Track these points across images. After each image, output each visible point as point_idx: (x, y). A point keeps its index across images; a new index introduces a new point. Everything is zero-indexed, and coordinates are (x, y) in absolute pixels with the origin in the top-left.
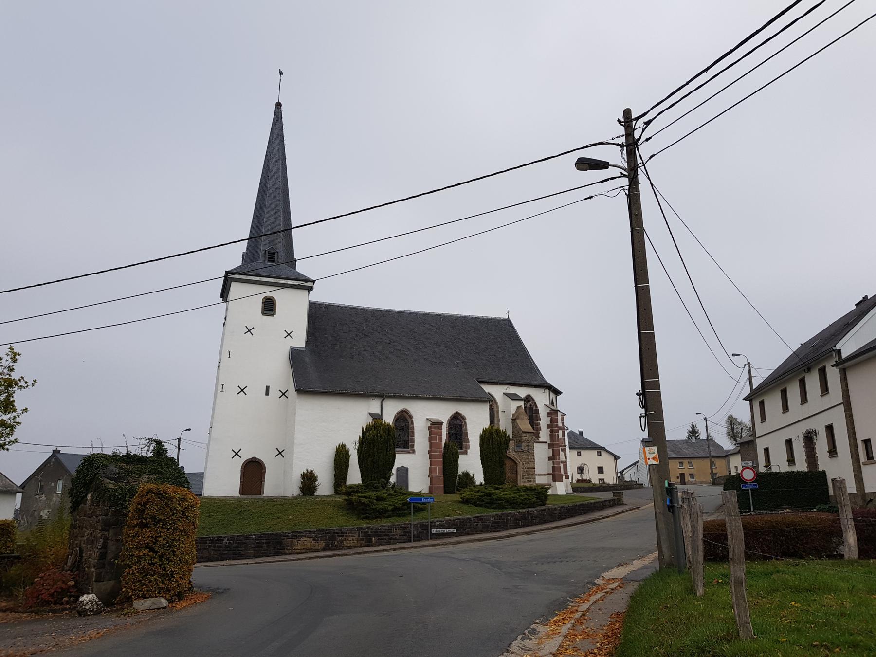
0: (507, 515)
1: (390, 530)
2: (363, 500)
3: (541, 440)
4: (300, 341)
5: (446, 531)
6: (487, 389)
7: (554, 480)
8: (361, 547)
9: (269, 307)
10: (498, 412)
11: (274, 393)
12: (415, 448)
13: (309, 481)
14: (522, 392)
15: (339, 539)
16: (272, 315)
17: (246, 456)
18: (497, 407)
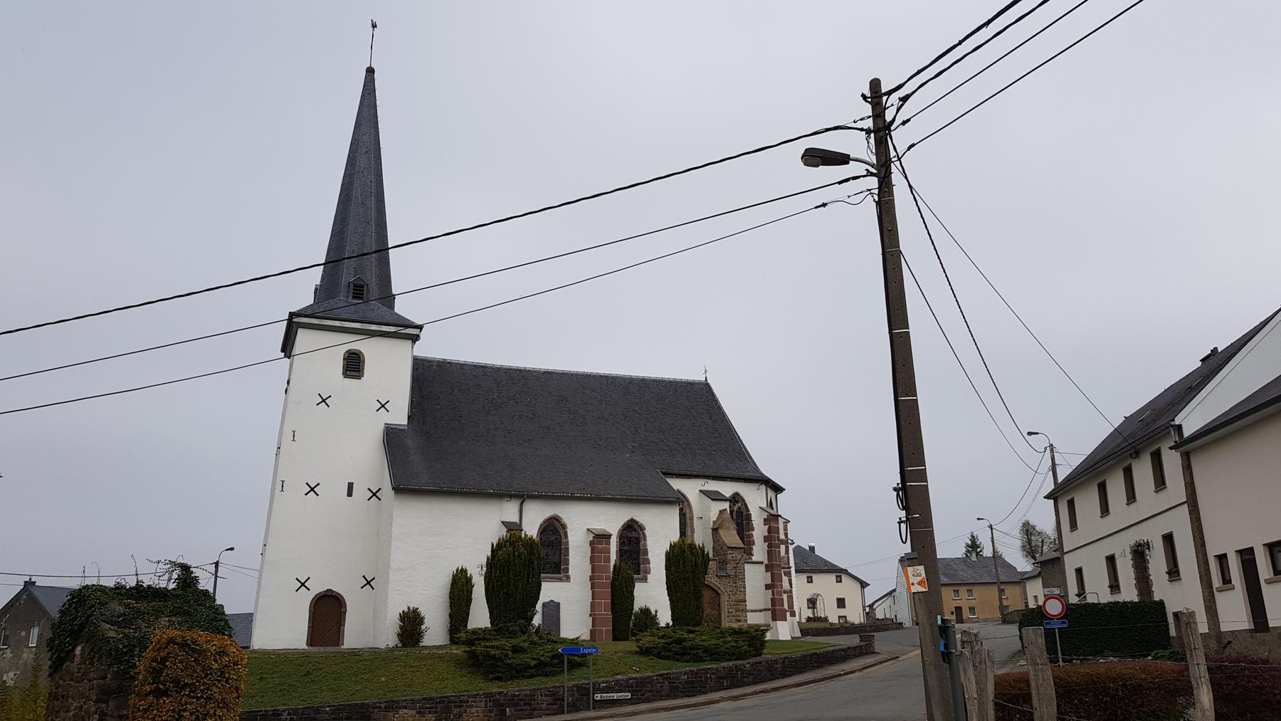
2: (493, 652)
3: (754, 559)
4: (399, 415)
5: (615, 696)
7: (774, 619)
9: (354, 365)
10: (692, 519)
11: (360, 492)
12: (570, 572)
13: (411, 623)
14: (727, 489)
15: (456, 711)
16: (359, 377)
17: (317, 588)
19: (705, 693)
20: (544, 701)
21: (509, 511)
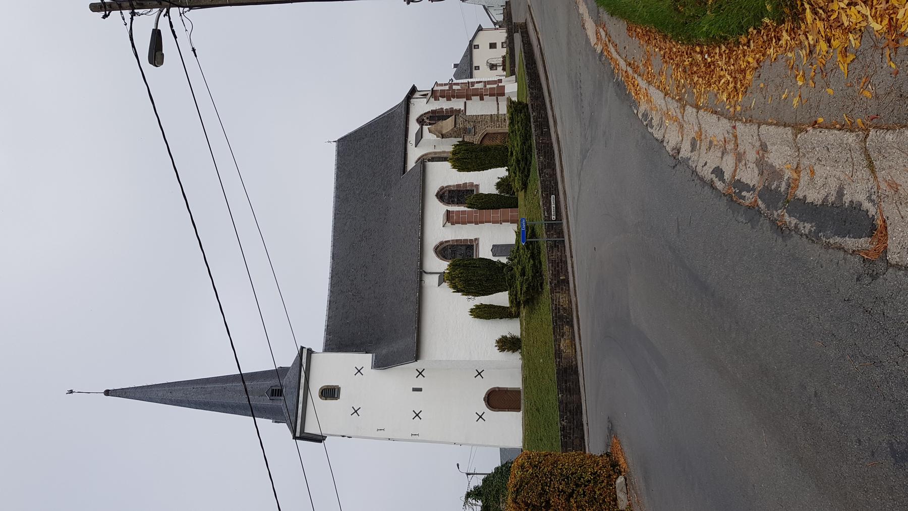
1: (553, 262)
2: (524, 289)
3: (463, 108)
4: (365, 359)
5: (553, 206)
6: (411, 164)
7: (503, 94)
8: (569, 290)
9: (330, 393)
10: (435, 153)
12: (473, 238)
13: (507, 344)
14: (414, 127)
16: (339, 389)
17: (483, 407)
18: (430, 153)
19: (552, 144)
20: (556, 254)
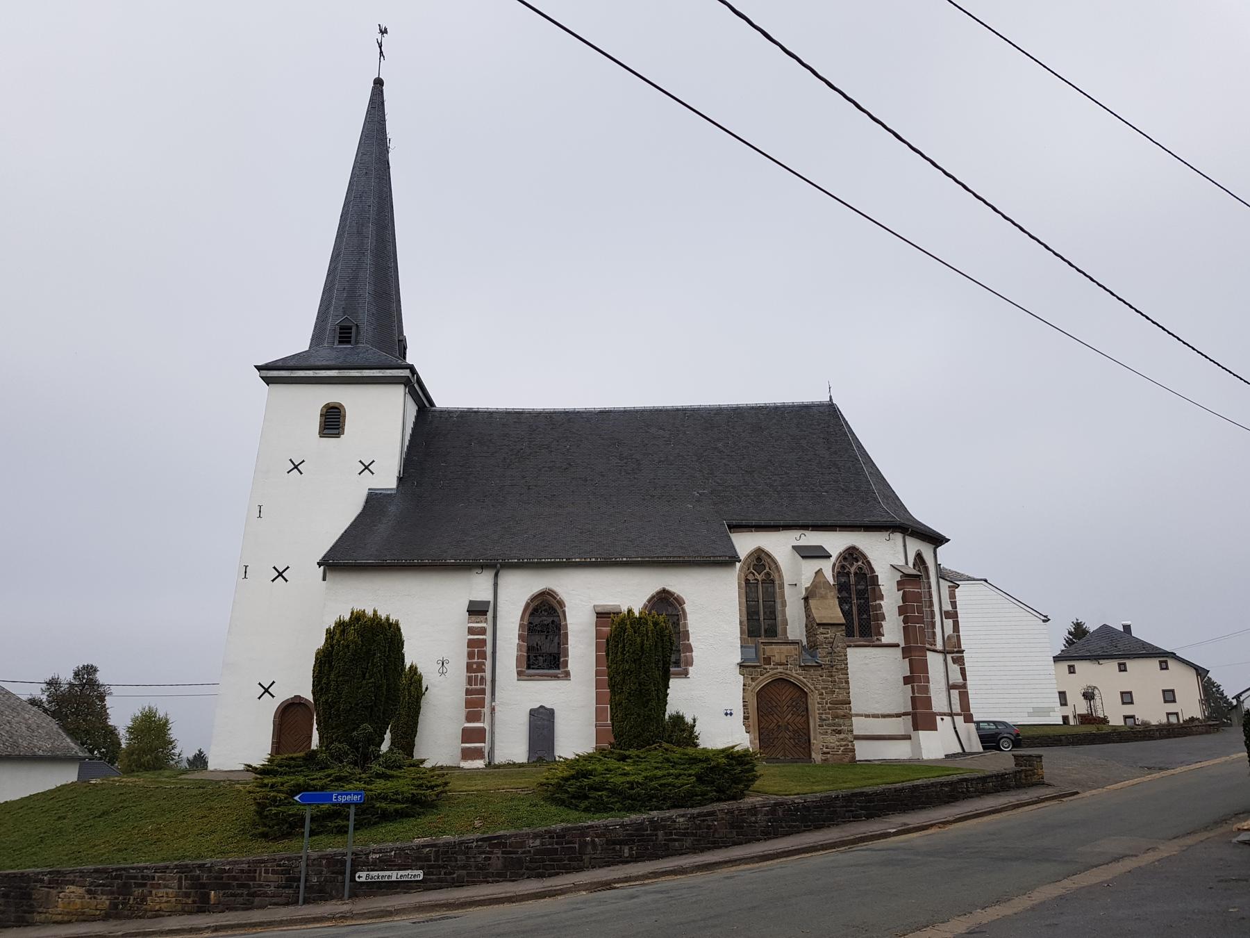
0: (583, 831)
1: (251, 873)
3: (884, 640)
4: (387, 478)
5: (395, 875)
7: (916, 728)
8: (184, 912)
9: (332, 421)
10: (782, 586)
12: (570, 667)
14: (835, 543)
16: (338, 435)
18: (781, 576)
19: (579, 869)
20: (270, 881)
21: (479, 586)
